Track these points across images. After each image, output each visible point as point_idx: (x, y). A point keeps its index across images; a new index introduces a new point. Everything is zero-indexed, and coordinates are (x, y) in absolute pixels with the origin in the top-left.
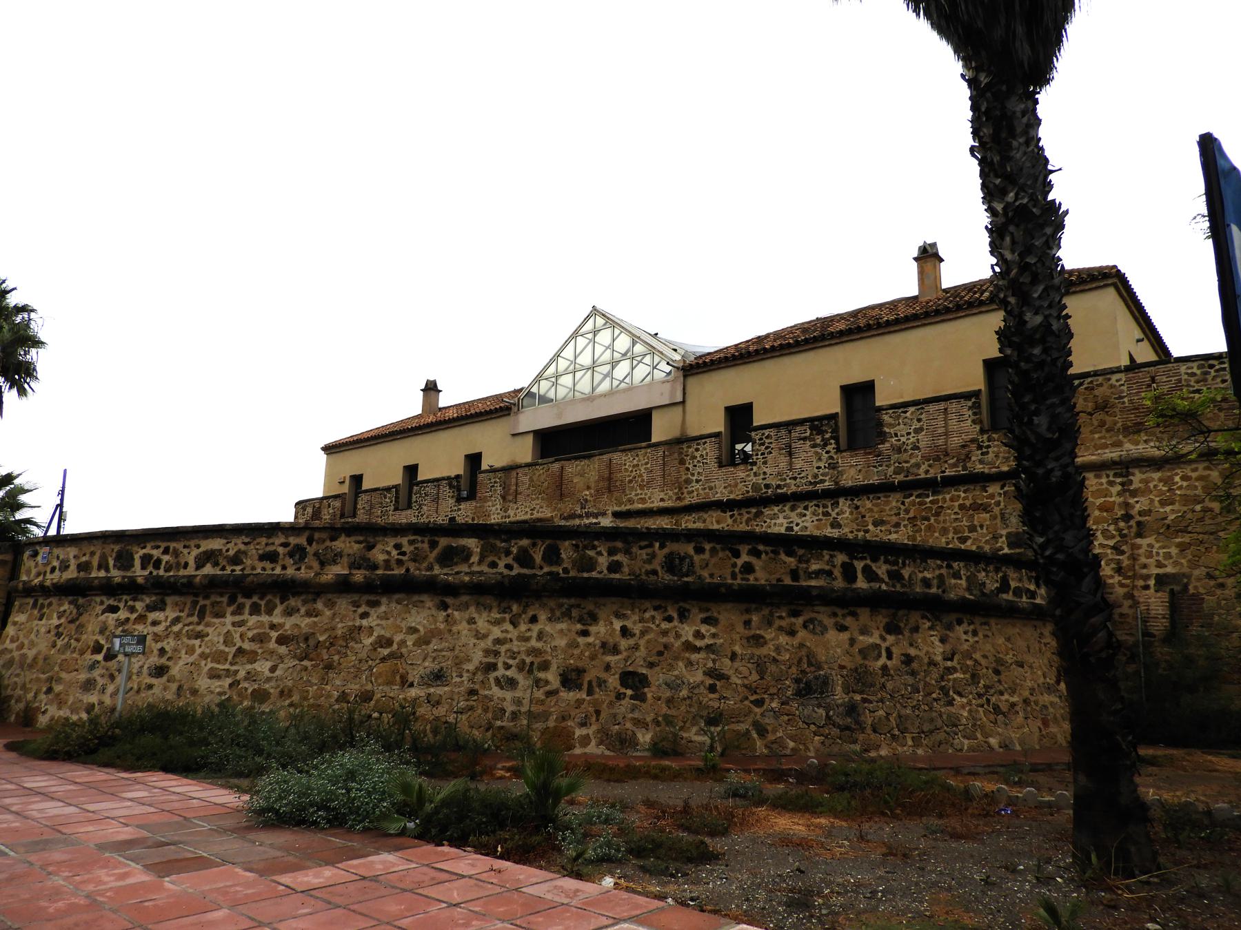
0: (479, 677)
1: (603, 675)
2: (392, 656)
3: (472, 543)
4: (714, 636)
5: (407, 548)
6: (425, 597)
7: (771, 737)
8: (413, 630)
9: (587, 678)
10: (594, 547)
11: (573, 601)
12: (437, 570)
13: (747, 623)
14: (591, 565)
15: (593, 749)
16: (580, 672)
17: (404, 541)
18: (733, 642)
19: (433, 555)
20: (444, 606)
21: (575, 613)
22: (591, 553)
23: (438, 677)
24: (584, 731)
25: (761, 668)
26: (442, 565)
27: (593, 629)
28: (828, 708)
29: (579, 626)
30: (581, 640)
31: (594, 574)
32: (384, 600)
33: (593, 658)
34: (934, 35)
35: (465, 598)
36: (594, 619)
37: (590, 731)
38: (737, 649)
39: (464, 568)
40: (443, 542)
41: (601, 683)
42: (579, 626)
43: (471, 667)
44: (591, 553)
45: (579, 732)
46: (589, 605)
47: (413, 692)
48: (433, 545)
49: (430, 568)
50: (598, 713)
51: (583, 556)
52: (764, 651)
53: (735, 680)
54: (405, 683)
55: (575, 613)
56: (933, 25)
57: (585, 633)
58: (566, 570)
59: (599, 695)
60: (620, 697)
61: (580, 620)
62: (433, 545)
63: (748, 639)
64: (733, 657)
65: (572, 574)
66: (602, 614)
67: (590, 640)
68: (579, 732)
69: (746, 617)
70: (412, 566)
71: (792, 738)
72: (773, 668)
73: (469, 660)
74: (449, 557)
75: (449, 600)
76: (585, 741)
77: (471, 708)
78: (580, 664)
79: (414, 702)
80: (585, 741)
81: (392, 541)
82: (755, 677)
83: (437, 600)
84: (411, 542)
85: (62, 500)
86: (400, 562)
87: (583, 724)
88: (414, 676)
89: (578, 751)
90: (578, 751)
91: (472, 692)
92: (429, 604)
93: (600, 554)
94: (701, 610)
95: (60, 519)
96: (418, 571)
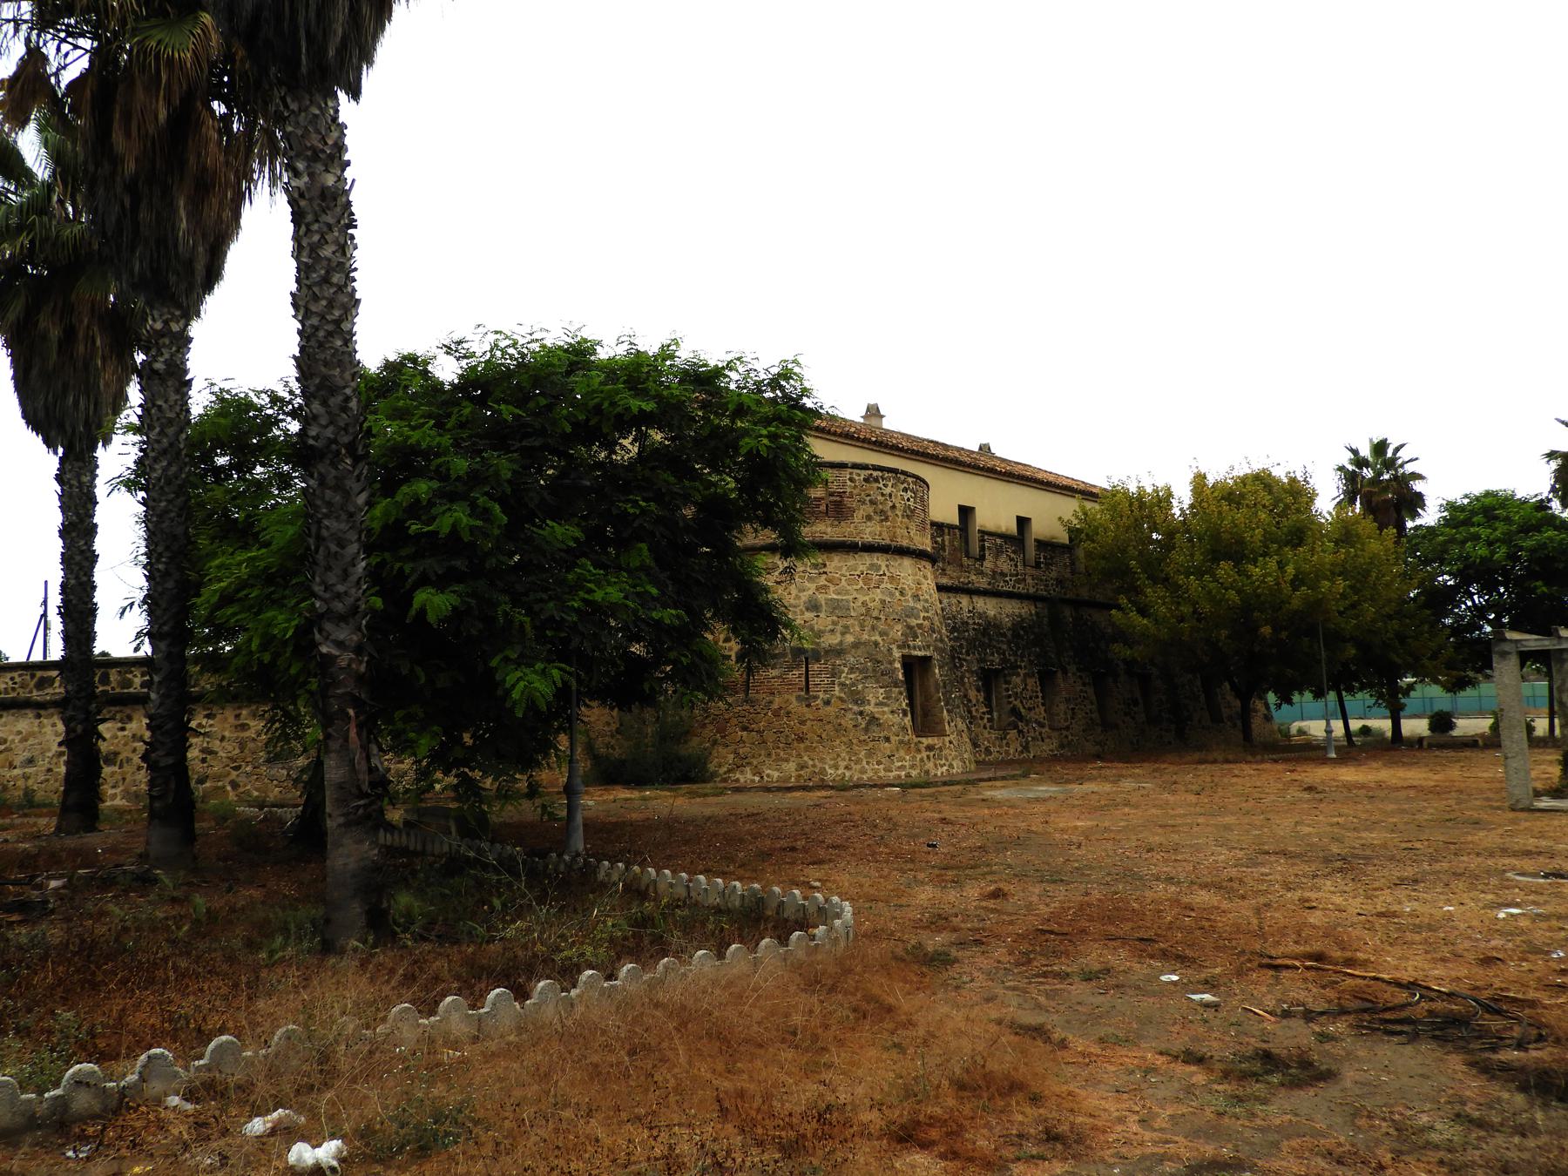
0: (55, 760)
1: (131, 755)
2: (6, 750)
3: (54, 673)
4: (211, 726)
5: (18, 680)
6: (28, 711)
7: (242, 790)
8: (19, 733)
9: (121, 757)
10: (131, 672)
11: (118, 708)
12: (35, 693)
13: (237, 716)
14: (129, 684)
15: (118, 802)
16: (116, 754)
17: (15, 675)
18: (224, 729)
19: (33, 683)
20: (39, 716)
21: (118, 716)
22: (130, 676)
23: (31, 761)
24: (114, 791)
25: (242, 745)
26: (38, 689)
27: (128, 726)
28: (289, 770)
29: (120, 725)
30: (120, 734)
31: (131, 690)
32: (5, 714)
33: (126, 744)
34: (11, 384)
35: (51, 710)
36: (130, 719)
37: (118, 791)
38: (227, 734)
39: (50, 691)
40: (39, 674)
41: (129, 760)
42: (120, 725)
43: (50, 754)
44: (130, 676)
45: (111, 792)
46: (128, 711)
47: (16, 772)
48: (33, 676)
49: (31, 692)
50: (124, 779)
51: (124, 679)
52: (247, 734)
53: (221, 754)
54: (12, 766)
55: (118, 716)
56: (14, 377)
57: (123, 729)
58: (113, 689)
59: (126, 768)
60: (139, 768)
61: (121, 721)
62: (33, 676)
63: (236, 727)
64: (223, 739)
65: (118, 690)
66: (136, 716)
67: (126, 733)
68: (111, 792)
69: (237, 712)
70: (21, 691)
71: (256, 790)
72: (251, 745)
73: (49, 750)
74: (43, 684)
75: (42, 712)
76: (114, 797)
77: (47, 780)
78: (117, 749)
79: (16, 778)
80: (114, 797)
81: (9, 675)
82: (237, 751)
83: (35, 712)
84: (20, 676)
85: (45, 611)
86: (13, 689)
87: (113, 787)
88: (17, 762)
89: (108, 804)
90: (108, 804)
91: (49, 770)
92: (31, 715)
93: (135, 676)
94: (205, 709)
95: (46, 628)
96: (24, 694)
